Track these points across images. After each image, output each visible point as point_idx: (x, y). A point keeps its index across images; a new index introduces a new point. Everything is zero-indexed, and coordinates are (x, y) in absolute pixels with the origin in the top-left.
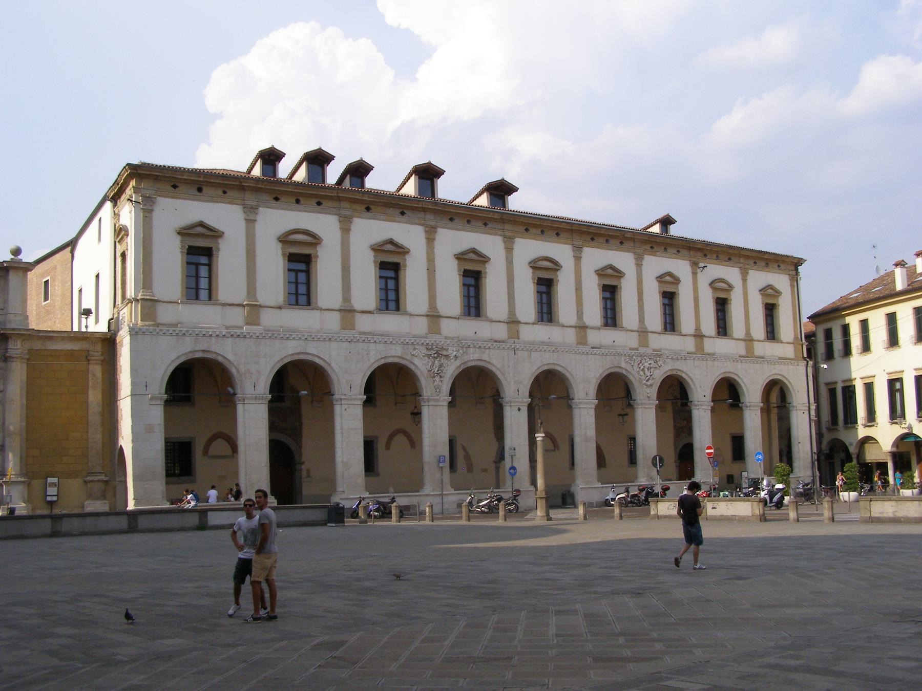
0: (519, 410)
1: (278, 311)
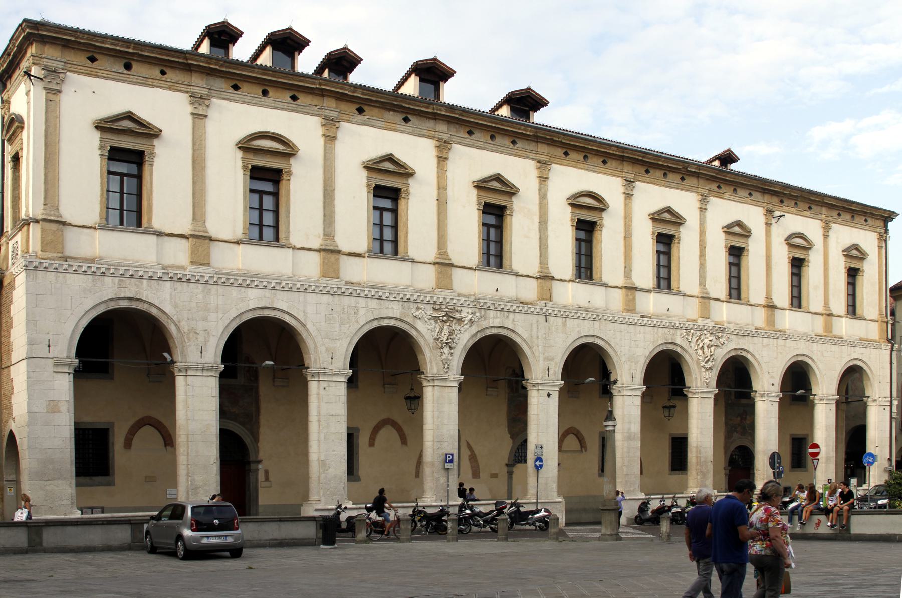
0: (549, 395)
1: (235, 246)
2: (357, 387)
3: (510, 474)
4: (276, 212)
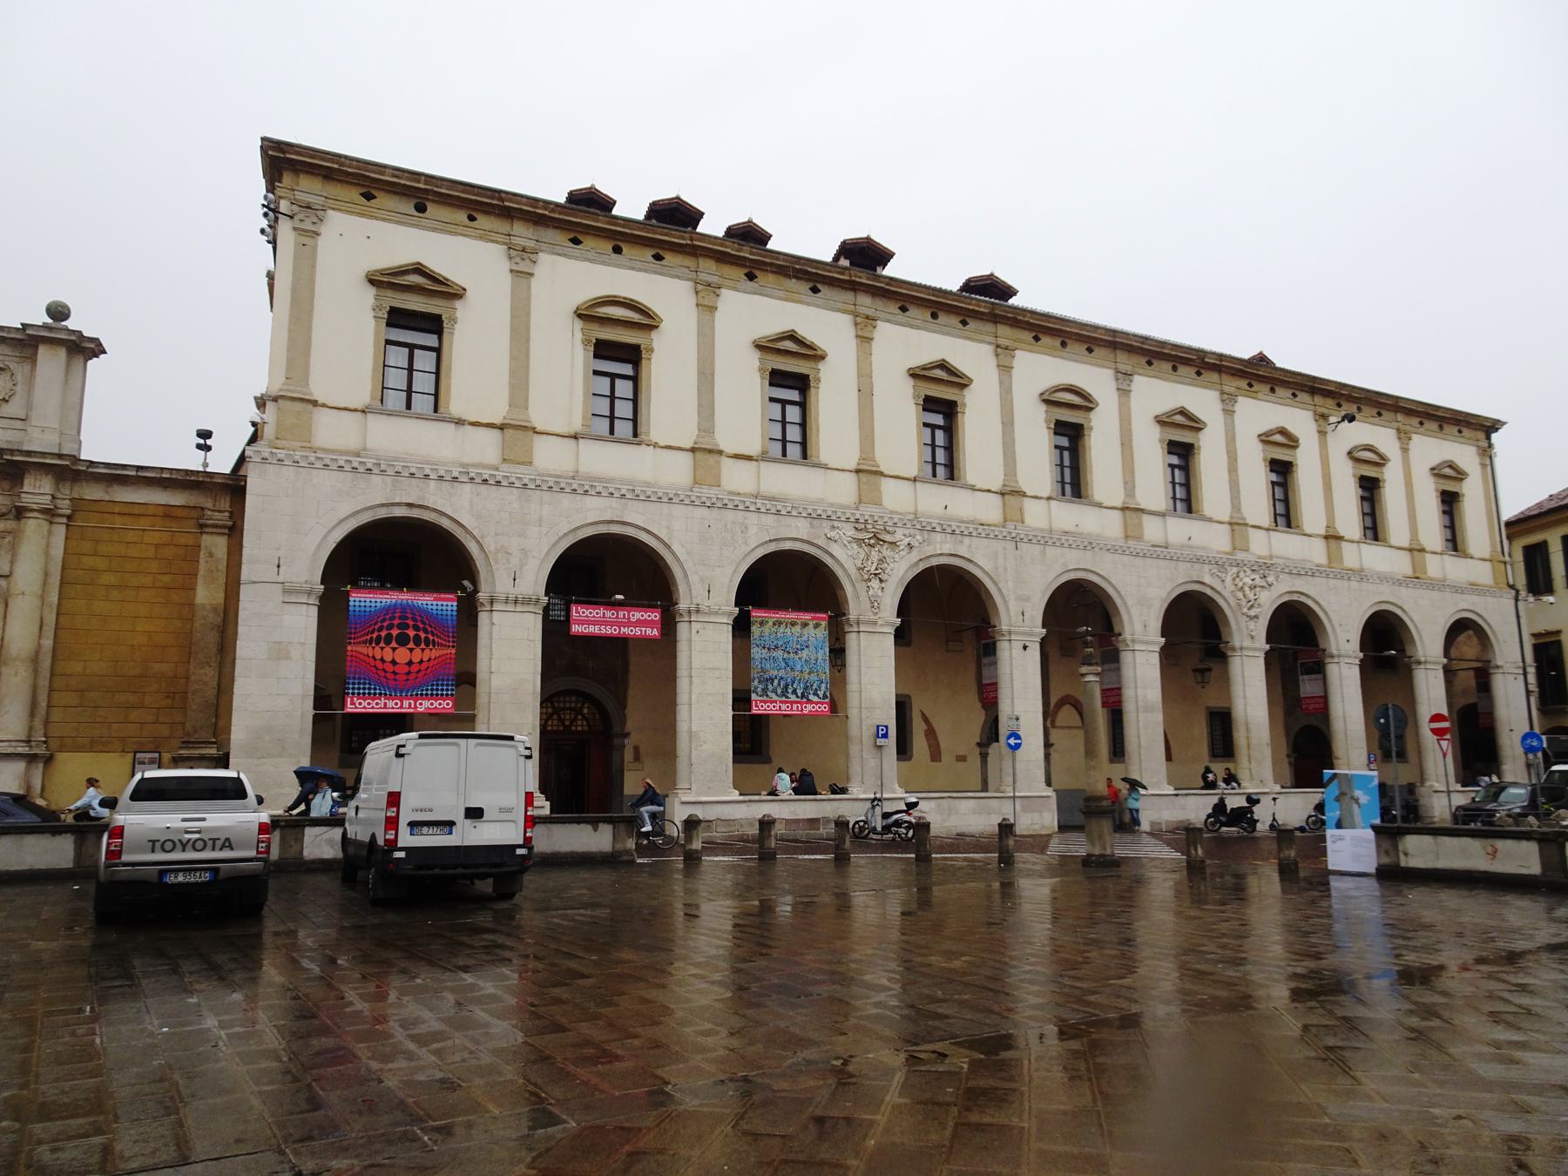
0: (1025, 648)
2: (908, 644)
3: (984, 757)
4: (803, 425)
